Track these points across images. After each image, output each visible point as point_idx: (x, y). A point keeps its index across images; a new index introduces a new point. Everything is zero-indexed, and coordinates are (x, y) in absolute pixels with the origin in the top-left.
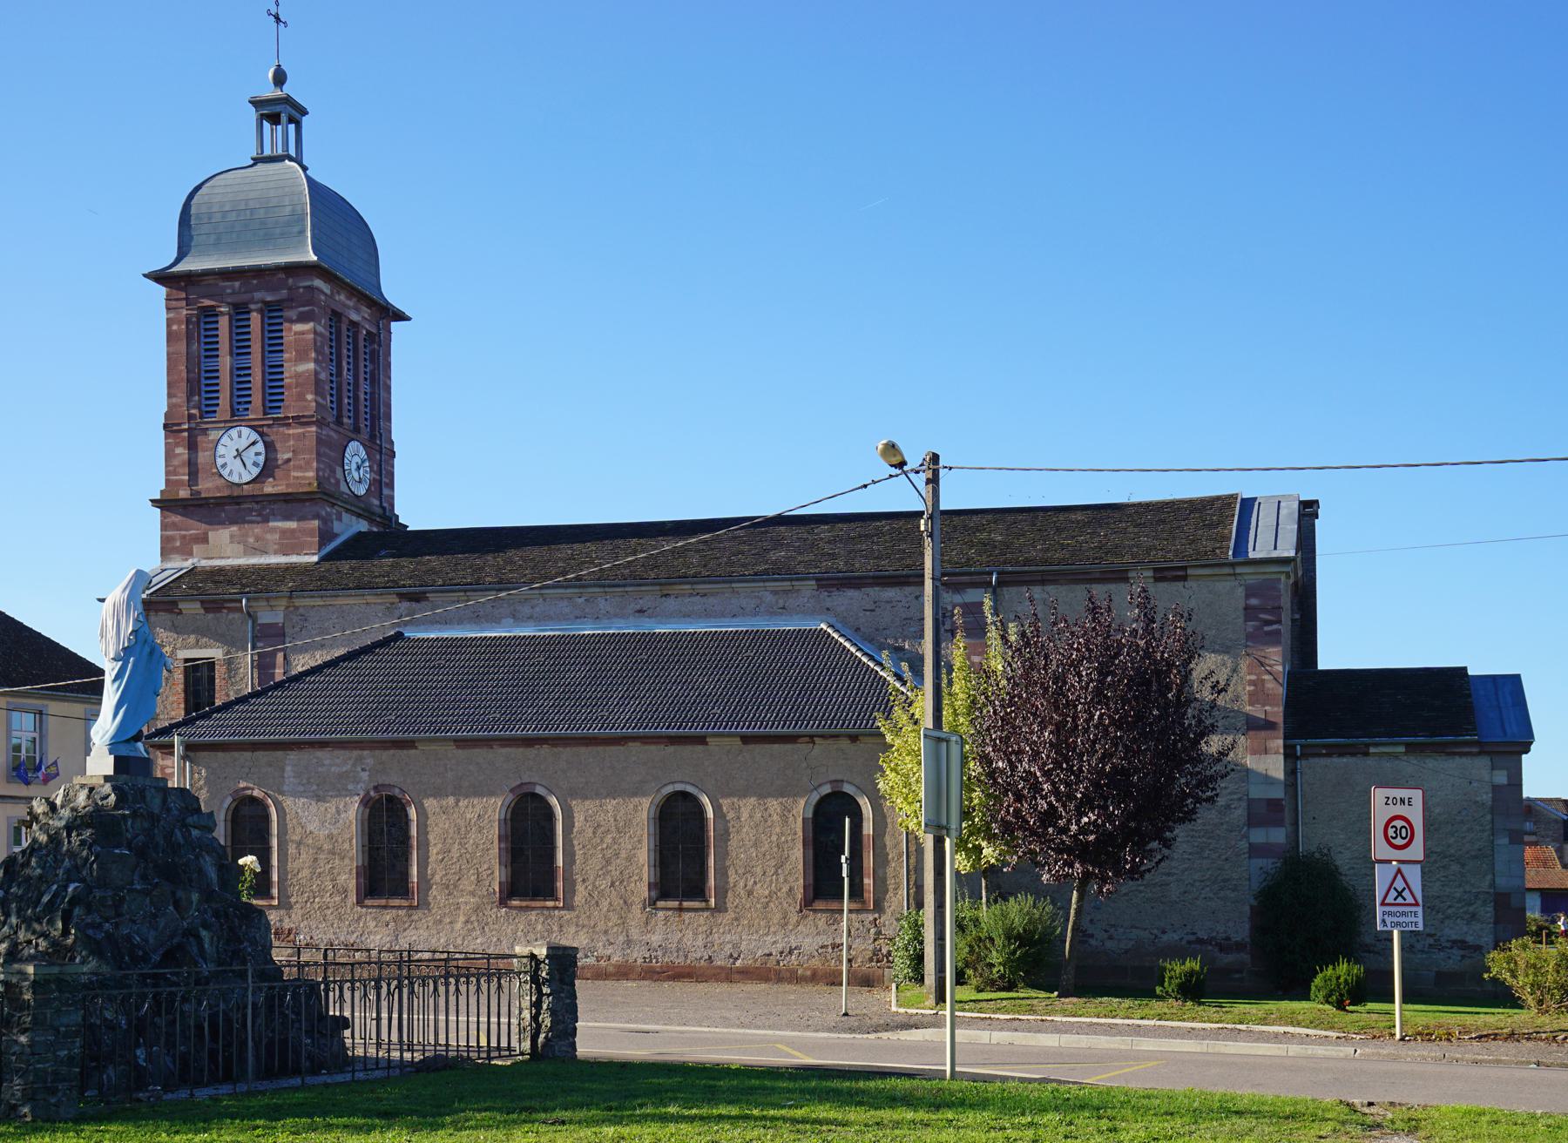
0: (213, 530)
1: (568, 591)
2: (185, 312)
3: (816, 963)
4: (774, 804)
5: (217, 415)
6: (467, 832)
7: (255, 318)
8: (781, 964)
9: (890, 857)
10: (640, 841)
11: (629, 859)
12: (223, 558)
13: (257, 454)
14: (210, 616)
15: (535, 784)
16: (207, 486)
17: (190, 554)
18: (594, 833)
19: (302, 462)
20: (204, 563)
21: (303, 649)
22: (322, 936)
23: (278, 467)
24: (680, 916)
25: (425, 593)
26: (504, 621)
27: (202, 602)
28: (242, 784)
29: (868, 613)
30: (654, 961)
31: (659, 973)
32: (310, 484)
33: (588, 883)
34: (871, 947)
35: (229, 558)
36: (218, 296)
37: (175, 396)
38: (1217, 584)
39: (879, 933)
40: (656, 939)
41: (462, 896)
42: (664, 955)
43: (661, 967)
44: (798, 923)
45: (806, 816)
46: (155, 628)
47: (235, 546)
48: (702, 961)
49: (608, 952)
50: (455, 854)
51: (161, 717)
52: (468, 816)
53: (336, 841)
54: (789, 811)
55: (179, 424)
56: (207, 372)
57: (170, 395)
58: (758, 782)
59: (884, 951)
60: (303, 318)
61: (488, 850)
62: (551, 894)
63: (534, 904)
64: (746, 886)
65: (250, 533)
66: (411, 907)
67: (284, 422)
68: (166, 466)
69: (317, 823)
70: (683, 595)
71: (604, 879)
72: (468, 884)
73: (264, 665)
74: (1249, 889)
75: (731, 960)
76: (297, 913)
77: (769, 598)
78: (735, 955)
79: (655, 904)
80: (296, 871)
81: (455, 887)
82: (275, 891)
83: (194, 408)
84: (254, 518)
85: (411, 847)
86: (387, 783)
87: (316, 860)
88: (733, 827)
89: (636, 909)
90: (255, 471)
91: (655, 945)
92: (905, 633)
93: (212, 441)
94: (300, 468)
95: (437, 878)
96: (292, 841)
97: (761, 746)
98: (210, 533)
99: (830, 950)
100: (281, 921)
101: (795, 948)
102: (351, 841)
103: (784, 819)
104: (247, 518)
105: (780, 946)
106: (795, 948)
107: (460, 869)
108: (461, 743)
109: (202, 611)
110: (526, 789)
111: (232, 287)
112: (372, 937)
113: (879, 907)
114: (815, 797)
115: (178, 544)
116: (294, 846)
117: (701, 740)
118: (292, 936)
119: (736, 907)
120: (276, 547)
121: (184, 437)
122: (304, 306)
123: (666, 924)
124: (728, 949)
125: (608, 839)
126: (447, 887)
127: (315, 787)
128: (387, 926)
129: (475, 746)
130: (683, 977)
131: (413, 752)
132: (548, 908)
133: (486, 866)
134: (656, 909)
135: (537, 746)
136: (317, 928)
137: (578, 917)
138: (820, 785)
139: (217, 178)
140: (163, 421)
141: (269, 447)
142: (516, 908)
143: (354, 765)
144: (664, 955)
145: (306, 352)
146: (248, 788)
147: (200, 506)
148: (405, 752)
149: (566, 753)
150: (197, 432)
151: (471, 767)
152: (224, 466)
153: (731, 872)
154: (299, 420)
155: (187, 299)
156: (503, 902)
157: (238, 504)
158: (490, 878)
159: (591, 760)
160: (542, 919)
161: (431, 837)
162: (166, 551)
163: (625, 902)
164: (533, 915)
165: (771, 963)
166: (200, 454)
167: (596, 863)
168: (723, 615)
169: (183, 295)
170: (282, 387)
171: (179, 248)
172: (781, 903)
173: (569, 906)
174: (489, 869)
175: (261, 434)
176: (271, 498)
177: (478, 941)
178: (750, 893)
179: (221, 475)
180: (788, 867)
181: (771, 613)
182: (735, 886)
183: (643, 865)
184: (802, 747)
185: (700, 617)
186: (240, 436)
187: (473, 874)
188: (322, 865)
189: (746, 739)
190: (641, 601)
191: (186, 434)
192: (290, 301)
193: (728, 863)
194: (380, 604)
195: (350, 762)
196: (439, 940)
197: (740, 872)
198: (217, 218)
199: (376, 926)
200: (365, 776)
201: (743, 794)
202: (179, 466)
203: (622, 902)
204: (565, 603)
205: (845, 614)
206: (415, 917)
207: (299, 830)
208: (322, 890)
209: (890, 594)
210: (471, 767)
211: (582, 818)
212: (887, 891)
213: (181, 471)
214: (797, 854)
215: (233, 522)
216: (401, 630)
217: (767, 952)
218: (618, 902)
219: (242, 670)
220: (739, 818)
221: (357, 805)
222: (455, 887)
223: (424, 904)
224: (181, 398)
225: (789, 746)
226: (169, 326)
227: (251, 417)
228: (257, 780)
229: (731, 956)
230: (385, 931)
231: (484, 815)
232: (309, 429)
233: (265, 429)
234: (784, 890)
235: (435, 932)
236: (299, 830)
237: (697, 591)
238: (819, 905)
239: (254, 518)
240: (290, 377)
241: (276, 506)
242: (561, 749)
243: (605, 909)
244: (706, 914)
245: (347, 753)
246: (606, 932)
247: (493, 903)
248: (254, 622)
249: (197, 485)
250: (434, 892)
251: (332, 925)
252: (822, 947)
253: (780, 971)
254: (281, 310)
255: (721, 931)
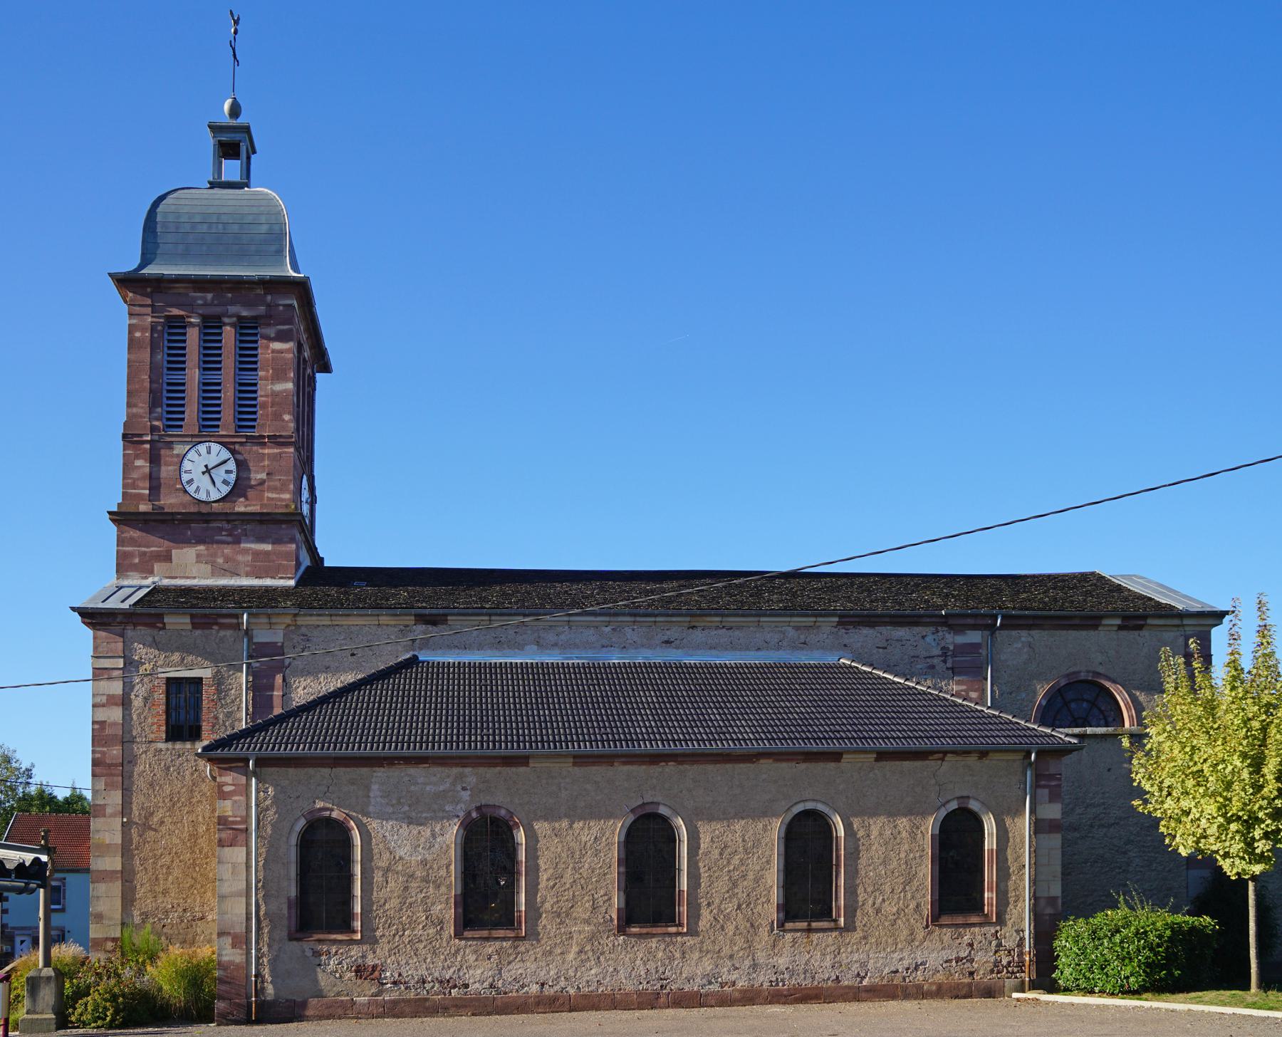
0: (177, 548)
1: (599, 619)
2: (150, 319)
3: (940, 977)
4: (903, 823)
5: (183, 430)
6: (582, 856)
7: (229, 334)
8: (907, 980)
9: (1011, 871)
10: (768, 862)
11: (757, 880)
12: (188, 578)
13: (228, 472)
14: (198, 632)
15: (658, 804)
16: (170, 501)
17: (151, 572)
18: (721, 854)
19: (277, 484)
20: (166, 582)
21: (306, 672)
22: (412, 972)
23: (251, 487)
24: (808, 937)
25: (446, 615)
26: (528, 647)
27: (192, 616)
28: (319, 804)
29: (881, 650)
30: (781, 984)
31: (785, 996)
32: (287, 506)
33: (713, 907)
34: (992, 959)
35: (195, 578)
36: (190, 306)
37: (135, 406)
38: (1164, 634)
39: (999, 945)
40: (782, 962)
41: (576, 924)
42: (791, 978)
43: (789, 990)
44: (925, 939)
45: (934, 833)
46: (132, 643)
47: (203, 566)
48: (830, 982)
49: (733, 977)
50: (568, 879)
51: (138, 740)
52: (584, 839)
53: (431, 867)
54: (918, 828)
55: (141, 435)
56: (169, 384)
57: (129, 405)
58: (888, 799)
59: (1004, 962)
60: (281, 337)
61: (605, 875)
62: (671, 919)
63: (654, 930)
64: (874, 904)
65: (219, 554)
66: (517, 938)
67: (259, 441)
68: (124, 478)
69: (408, 847)
70: (710, 628)
71: (730, 902)
72: (581, 911)
73: (260, 689)
74: (1187, 896)
75: (858, 979)
76: (383, 949)
77: (791, 633)
78: (862, 974)
79: (783, 925)
80: (383, 901)
81: (567, 916)
82: (357, 924)
83: (157, 419)
84: (224, 538)
85: (519, 873)
86: (491, 803)
87: (406, 888)
88: (863, 845)
89: (764, 932)
90: (225, 490)
91: (782, 968)
92: (913, 670)
93: (178, 455)
94: (274, 489)
95: (547, 906)
96: (378, 868)
97: (893, 763)
98: (173, 551)
99: (954, 963)
100: (363, 957)
101: (921, 964)
102: (448, 866)
103: (913, 836)
104: (216, 538)
105: (906, 963)
106: (921, 964)
107: (574, 896)
108: (581, 760)
109: (190, 627)
110: (649, 810)
111: (204, 298)
112: (471, 972)
113: (1001, 921)
114: (943, 813)
115: (137, 561)
116: (380, 873)
117: (836, 756)
118: (376, 973)
119: (865, 926)
120: (248, 569)
121: (145, 449)
122: (284, 324)
123: (793, 946)
124: (855, 968)
125: (736, 861)
126: (559, 916)
127: (406, 808)
128: (489, 959)
129: (594, 764)
130: (811, 999)
131: (522, 769)
132: (670, 934)
133: (602, 892)
134: (784, 931)
135: (663, 764)
136: (407, 963)
137: (702, 942)
138: (948, 802)
139: (180, 192)
140: (121, 430)
141: (241, 465)
142: (635, 935)
143: (454, 784)
144: (791, 978)
145: (285, 372)
146: (327, 809)
147: (163, 521)
148: (514, 769)
149: (692, 770)
150: (160, 445)
151: (588, 786)
152: (190, 482)
153: (860, 890)
154: (276, 440)
155: (152, 306)
156: (621, 930)
157: (207, 522)
158: (607, 904)
159: (719, 778)
160: (663, 946)
161: (541, 862)
162: (123, 566)
163: (752, 925)
164: (653, 943)
165: (897, 980)
166: (163, 468)
167: (722, 885)
168: (747, 649)
169: (149, 302)
170: (255, 406)
171: (143, 254)
172: (908, 920)
173: (693, 932)
174: (605, 895)
175: (233, 452)
176: (241, 518)
177: (593, 972)
178: (878, 911)
179: (186, 491)
180: (916, 883)
181: (794, 647)
182: (863, 905)
183: (771, 887)
184: (931, 764)
185: (726, 649)
186: (209, 452)
187: (588, 901)
188: (413, 894)
189: (882, 756)
190: (668, 633)
191: (148, 446)
192: (268, 319)
193: (858, 881)
194: (395, 626)
195: (449, 781)
196: (548, 973)
197: (869, 890)
198: (187, 228)
199: (476, 960)
200: (466, 795)
201: (874, 813)
202: (138, 479)
203: (748, 925)
204: (592, 631)
205: (861, 651)
206: (522, 949)
207: (386, 856)
208: (413, 923)
209: (900, 633)
210: (588, 786)
211: (708, 839)
212: (1008, 904)
213: (141, 484)
214: (926, 871)
215: (200, 541)
216: (416, 653)
217: (893, 969)
218: (744, 925)
219: (233, 691)
220: (868, 836)
221: (456, 828)
222: (567, 916)
223: (533, 935)
224: (142, 409)
225: (918, 764)
226: (130, 332)
227: (221, 433)
228: (336, 800)
229: (858, 974)
230: (487, 964)
231: (601, 838)
232: (286, 450)
233: (237, 447)
234: (911, 906)
235: (544, 964)
236: (386, 856)
237: (724, 624)
238: (945, 920)
239: (224, 538)
240: (266, 396)
241: (248, 527)
242: (687, 766)
243: (731, 933)
244: (834, 934)
245: (446, 770)
246: (731, 957)
247: (609, 931)
248: (249, 641)
249: (159, 501)
250: (544, 921)
251: (425, 960)
252: (946, 962)
253: (907, 987)
254: (256, 328)
255: (849, 950)
